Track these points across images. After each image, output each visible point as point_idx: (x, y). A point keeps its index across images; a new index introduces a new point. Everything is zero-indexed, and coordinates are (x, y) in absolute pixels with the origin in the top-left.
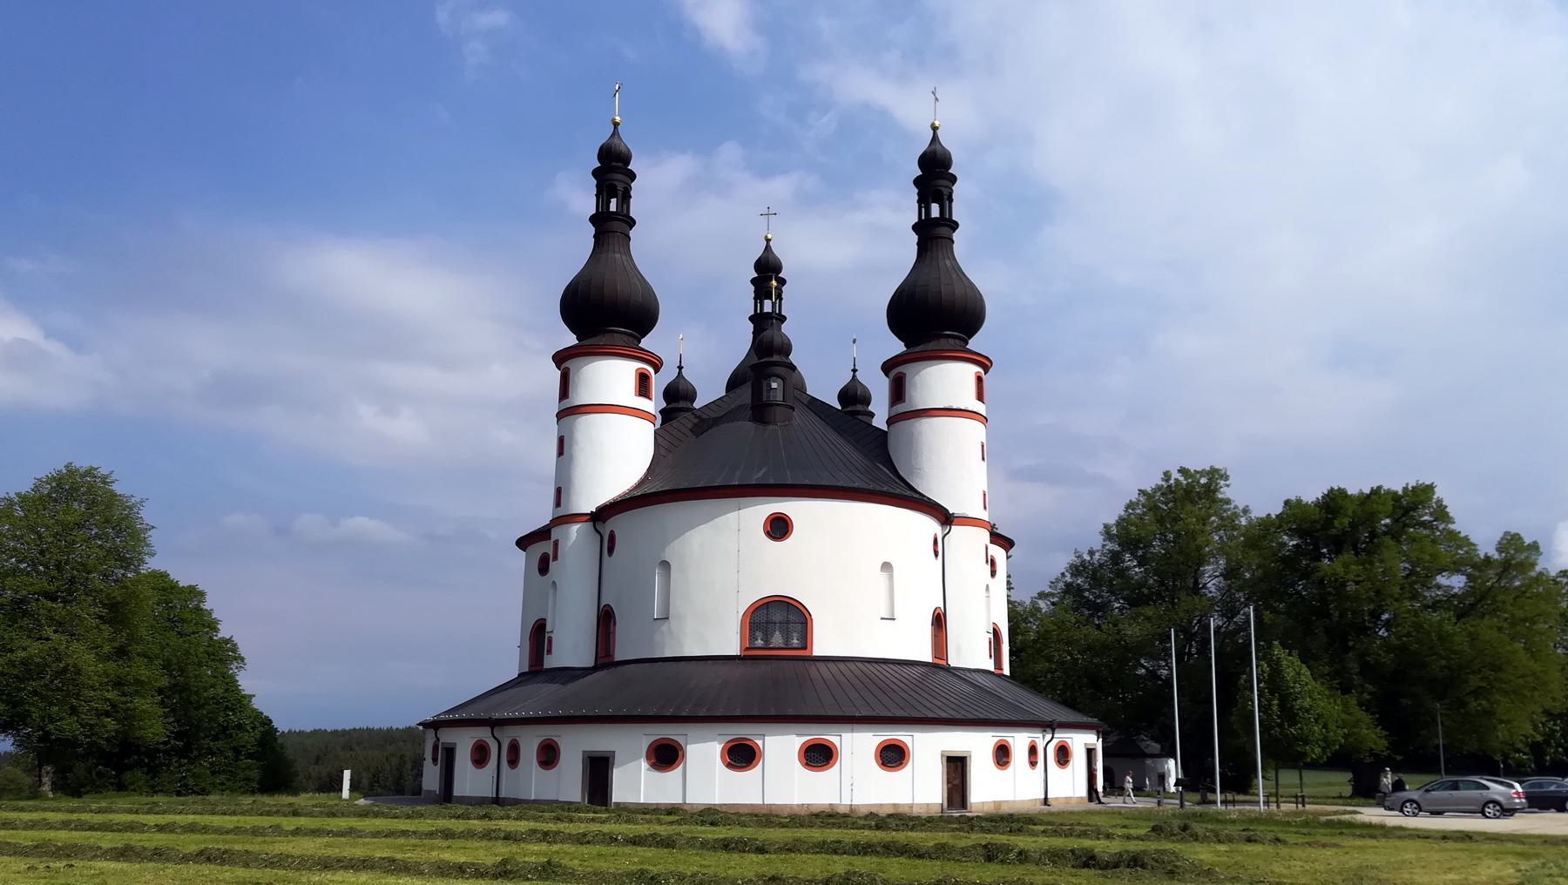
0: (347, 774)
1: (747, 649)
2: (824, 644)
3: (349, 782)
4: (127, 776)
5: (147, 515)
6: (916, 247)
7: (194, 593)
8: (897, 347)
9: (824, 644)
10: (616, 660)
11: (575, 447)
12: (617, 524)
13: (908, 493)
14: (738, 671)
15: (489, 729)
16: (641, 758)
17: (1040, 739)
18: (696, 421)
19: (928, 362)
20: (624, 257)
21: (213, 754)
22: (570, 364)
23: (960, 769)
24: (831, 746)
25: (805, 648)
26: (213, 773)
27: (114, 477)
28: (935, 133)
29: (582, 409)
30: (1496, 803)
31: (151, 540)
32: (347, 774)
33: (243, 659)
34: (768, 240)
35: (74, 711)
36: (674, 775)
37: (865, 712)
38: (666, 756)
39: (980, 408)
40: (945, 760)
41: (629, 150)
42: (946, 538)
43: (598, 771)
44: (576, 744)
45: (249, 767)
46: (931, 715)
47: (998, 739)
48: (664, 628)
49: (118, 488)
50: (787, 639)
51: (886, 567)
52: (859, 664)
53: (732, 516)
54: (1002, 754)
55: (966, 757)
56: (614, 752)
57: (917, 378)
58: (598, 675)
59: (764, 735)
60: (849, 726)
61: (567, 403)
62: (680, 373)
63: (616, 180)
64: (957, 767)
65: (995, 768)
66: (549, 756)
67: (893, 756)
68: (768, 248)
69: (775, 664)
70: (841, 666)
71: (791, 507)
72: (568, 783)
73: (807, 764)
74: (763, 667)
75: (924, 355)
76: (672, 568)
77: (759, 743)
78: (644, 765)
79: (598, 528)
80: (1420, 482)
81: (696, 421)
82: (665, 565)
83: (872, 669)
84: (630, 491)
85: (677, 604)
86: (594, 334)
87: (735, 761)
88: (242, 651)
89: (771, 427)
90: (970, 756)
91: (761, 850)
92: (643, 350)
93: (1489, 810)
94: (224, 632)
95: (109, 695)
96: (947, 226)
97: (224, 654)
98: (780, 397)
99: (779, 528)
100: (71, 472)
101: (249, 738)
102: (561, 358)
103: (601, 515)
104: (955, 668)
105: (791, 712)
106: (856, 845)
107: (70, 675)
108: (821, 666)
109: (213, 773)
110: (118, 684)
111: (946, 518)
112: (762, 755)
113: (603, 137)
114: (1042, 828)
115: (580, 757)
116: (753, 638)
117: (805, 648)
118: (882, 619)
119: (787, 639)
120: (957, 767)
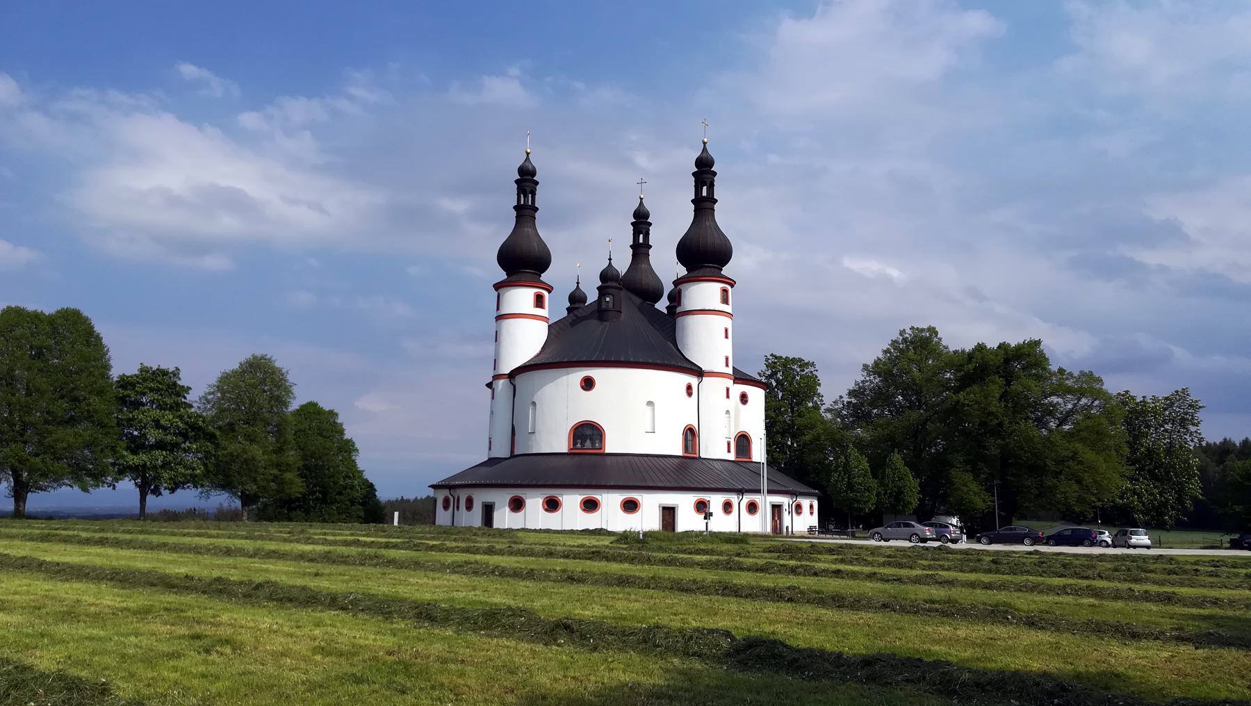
0: (396, 514)
1: (571, 449)
2: (613, 445)
3: (1089, 553)
4: (293, 514)
5: (291, 378)
7: (332, 414)
8: (502, 275)
9: (613, 445)
11: (502, 337)
12: (519, 379)
14: (567, 460)
15: (448, 491)
16: (504, 506)
17: (734, 498)
18: (574, 318)
21: (338, 503)
22: (501, 291)
23: (672, 514)
25: (601, 449)
26: (339, 513)
27: (273, 359)
28: (704, 146)
29: (506, 316)
30: (917, 535)
31: (294, 391)
32: (396, 514)
33: (358, 451)
34: (641, 199)
35: (255, 480)
36: (521, 514)
38: (517, 505)
39: (728, 308)
40: (661, 509)
41: (534, 167)
43: (488, 510)
44: (481, 497)
45: (359, 510)
46: (692, 486)
47: (697, 498)
48: (533, 437)
49: (277, 365)
50: (593, 444)
51: (650, 403)
52: (656, 459)
53: (565, 378)
54: (727, 507)
57: (687, 292)
58: (511, 460)
60: (607, 490)
62: (578, 286)
63: (526, 186)
64: (669, 513)
66: (469, 504)
67: (630, 506)
68: (641, 203)
70: (624, 458)
71: (594, 373)
72: (475, 518)
74: (577, 458)
75: (692, 279)
76: (537, 405)
77: (560, 498)
78: (507, 509)
80: (1032, 339)
81: (574, 318)
82: (534, 403)
83: (663, 461)
84: (536, 357)
85: (539, 427)
86: (512, 275)
88: (357, 446)
89: (605, 323)
91: (815, 574)
92: (544, 283)
93: (914, 538)
94: (347, 436)
95: (272, 472)
96: (711, 202)
97: (348, 448)
98: (611, 305)
99: (588, 384)
100: (254, 357)
101: (358, 494)
103: (512, 375)
104: (704, 459)
105: (603, 484)
106: (1159, 594)
107: (249, 463)
108: (610, 457)
109: (339, 513)
110: (278, 465)
111: (699, 373)
113: (520, 162)
114: (882, 560)
115: (481, 506)
117: (601, 449)
119: (593, 444)
120: (669, 513)
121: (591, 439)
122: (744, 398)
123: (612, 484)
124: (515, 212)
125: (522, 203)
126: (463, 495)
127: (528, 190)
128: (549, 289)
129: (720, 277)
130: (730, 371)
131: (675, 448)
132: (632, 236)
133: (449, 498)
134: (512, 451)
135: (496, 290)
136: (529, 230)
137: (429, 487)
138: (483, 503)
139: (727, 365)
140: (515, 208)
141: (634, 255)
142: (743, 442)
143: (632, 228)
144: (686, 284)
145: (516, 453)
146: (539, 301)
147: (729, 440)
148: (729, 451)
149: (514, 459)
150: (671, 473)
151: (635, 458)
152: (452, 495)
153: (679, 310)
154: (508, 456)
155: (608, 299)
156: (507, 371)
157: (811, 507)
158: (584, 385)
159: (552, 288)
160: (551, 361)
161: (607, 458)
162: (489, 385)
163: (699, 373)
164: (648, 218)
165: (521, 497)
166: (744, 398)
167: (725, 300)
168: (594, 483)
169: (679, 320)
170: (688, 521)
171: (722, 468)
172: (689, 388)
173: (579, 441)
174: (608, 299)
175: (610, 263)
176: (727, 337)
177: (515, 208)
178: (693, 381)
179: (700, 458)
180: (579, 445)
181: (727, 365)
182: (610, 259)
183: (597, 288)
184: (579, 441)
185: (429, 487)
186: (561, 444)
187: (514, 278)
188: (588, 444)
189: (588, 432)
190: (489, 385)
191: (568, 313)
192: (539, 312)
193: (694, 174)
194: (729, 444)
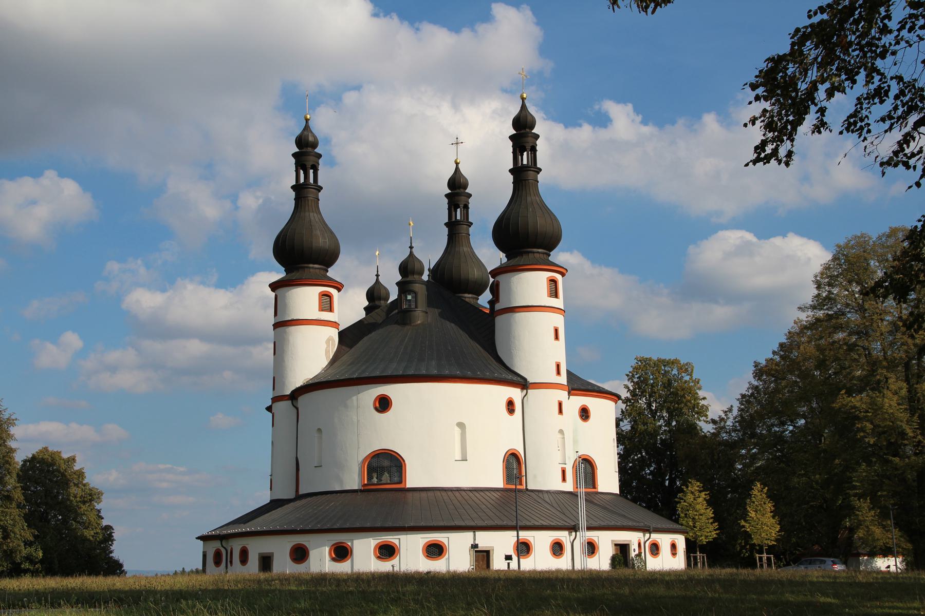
1: (365, 485)
2: (414, 478)
6: (294, 201)
8: (279, 274)
9: (414, 478)
10: (408, 486)
12: (302, 400)
13: (515, 378)
17: (563, 536)
19: (293, 287)
20: (315, 215)
24: (393, 545)
25: (400, 482)
28: (523, 101)
37: (490, 523)
39: (558, 303)
40: (614, 545)
42: (296, 411)
44: (256, 547)
51: (461, 425)
55: (629, 544)
56: (273, 553)
59: (353, 540)
61: (280, 319)
65: (551, 556)
66: (244, 556)
69: (384, 494)
73: (427, 556)
76: (322, 430)
77: (349, 544)
79: (294, 404)
87: (430, 555)
90: (493, 550)
99: (384, 404)
102: (274, 286)
104: (532, 491)
108: (416, 494)
111: (523, 384)
112: (399, 550)
115: (257, 557)
116: (370, 478)
117: (400, 482)
118: (456, 460)
121: (389, 473)
122: (585, 413)
123: (412, 524)
124: (294, 193)
125: (302, 180)
126: (236, 546)
127: (309, 164)
128: (339, 288)
129: (549, 265)
130: (563, 380)
131: (495, 479)
132: (447, 211)
133: (220, 550)
134: (297, 490)
135: (273, 290)
136: (313, 216)
137: (198, 538)
138: (259, 554)
139: (558, 373)
140: (293, 187)
141: (515, 183)
142: (587, 467)
143: (511, 143)
144: (506, 274)
145: (301, 492)
146: (327, 303)
147: (564, 466)
148: (564, 479)
149: (303, 501)
150: (486, 510)
151: (444, 494)
152: (224, 548)
153: (498, 307)
154: (293, 497)
155: (409, 297)
156: (288, 392)
157: (674, 546)
158: (378, 405)
159: (342, 286)
160: (338, 377)
161: (410, 495)
162: (269, 409)
163: (523, 384)
164: (533, 127)
165: (303, 544)
166: (585, 413)
167: (554, 293)
168: (389, 524)
169: (500, 320)
170: (284, 565)
171: (553, 502)
172: (510, 406)
173: (375, 475)
174: (409, 297)
175: (377, 280)
176: (557, 338)
177: (293, 187)
178: (515, 393)
179: (527, 489)
180: (375, 480)
181: (558, 373)
182: (411, 247)
183: (396, 284)
184: (375, 475)
185: (198, 538)
186: (353, 480)
187: (295, 275)
188: (386, 477)
189: (386, 463)
190: (269, 409)
191: (366, 314)
192: (553, 302)
193: (511, 137)
194: (564, 472)
